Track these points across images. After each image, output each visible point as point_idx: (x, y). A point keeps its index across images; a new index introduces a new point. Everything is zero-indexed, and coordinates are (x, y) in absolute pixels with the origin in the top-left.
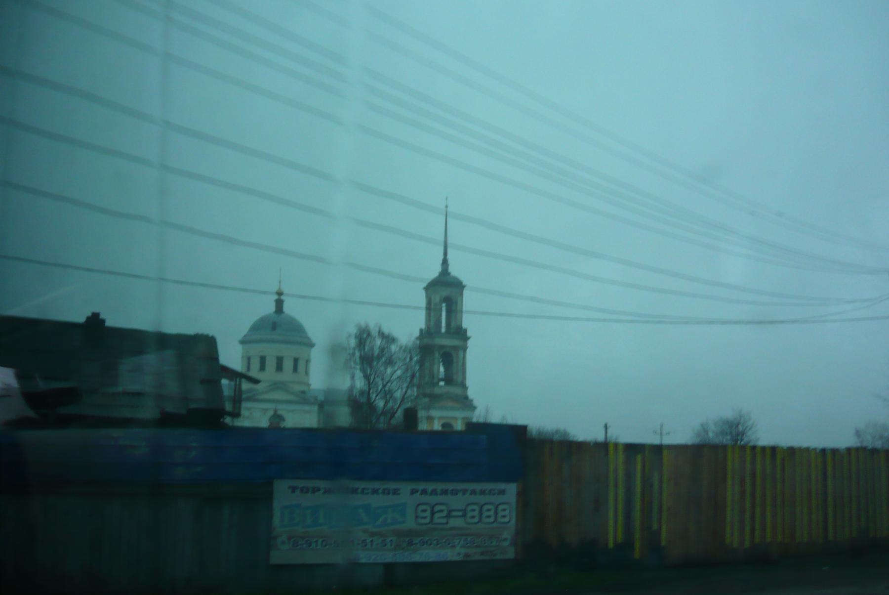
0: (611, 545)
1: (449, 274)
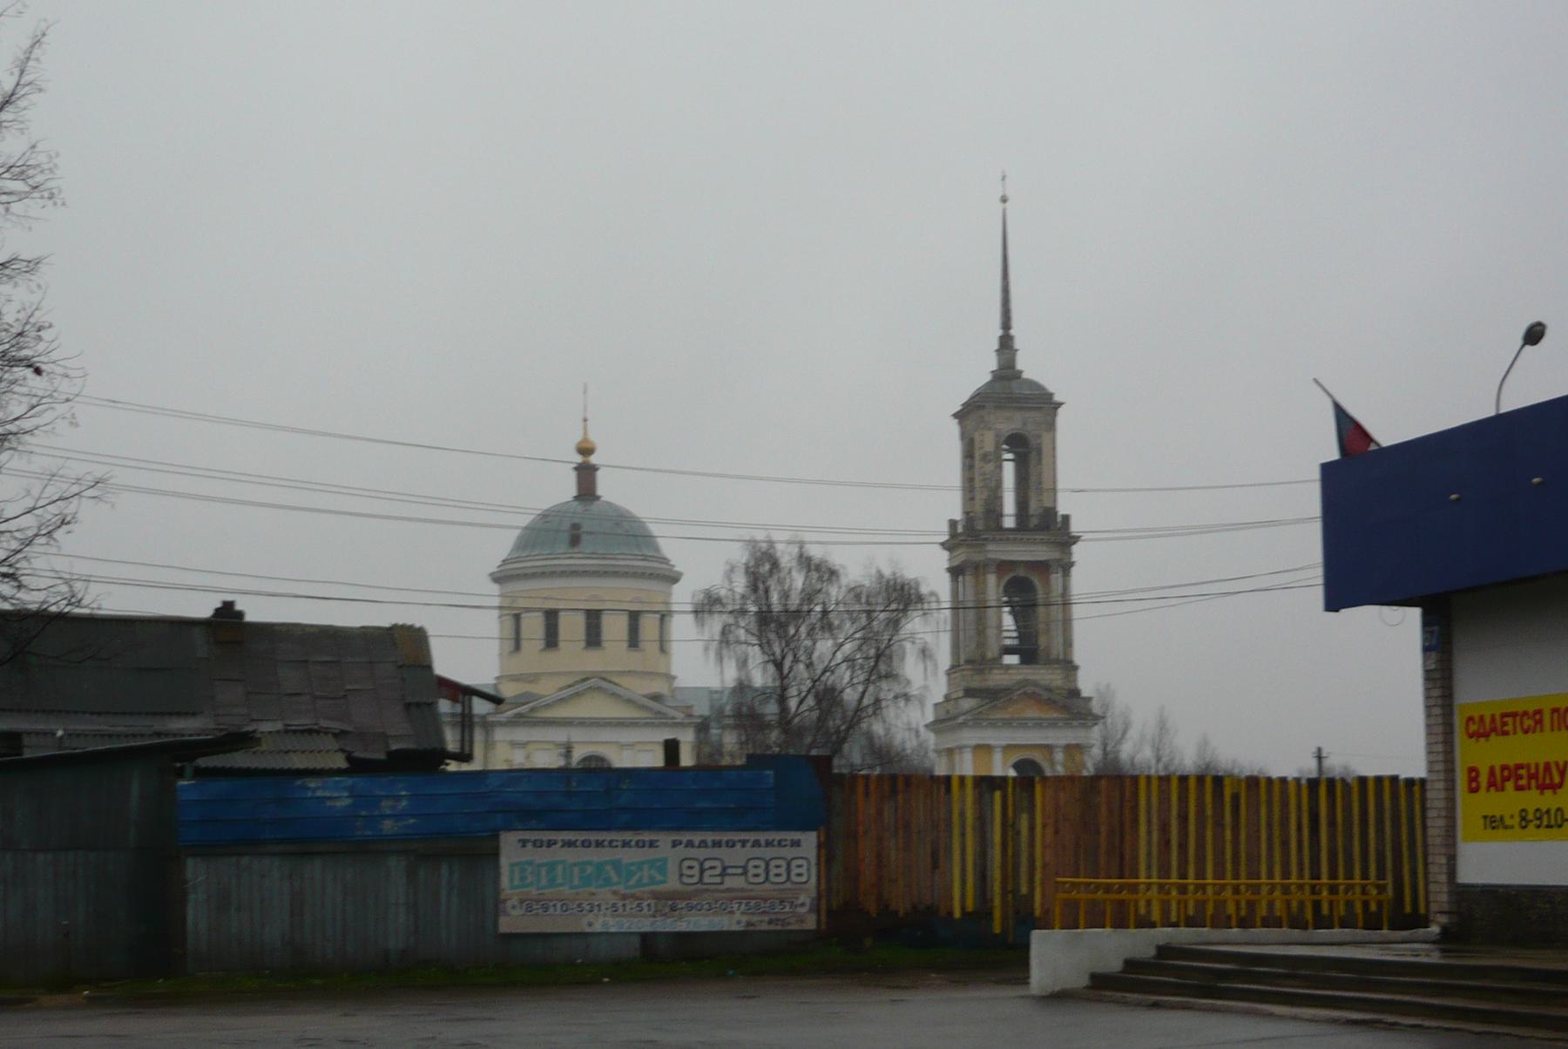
0: (957, 914)
1: (1017, 375)
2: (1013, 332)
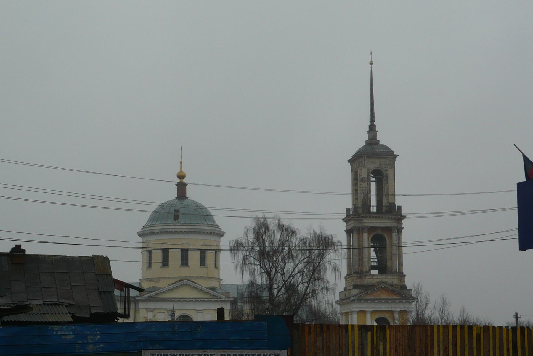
1: (377, 143)
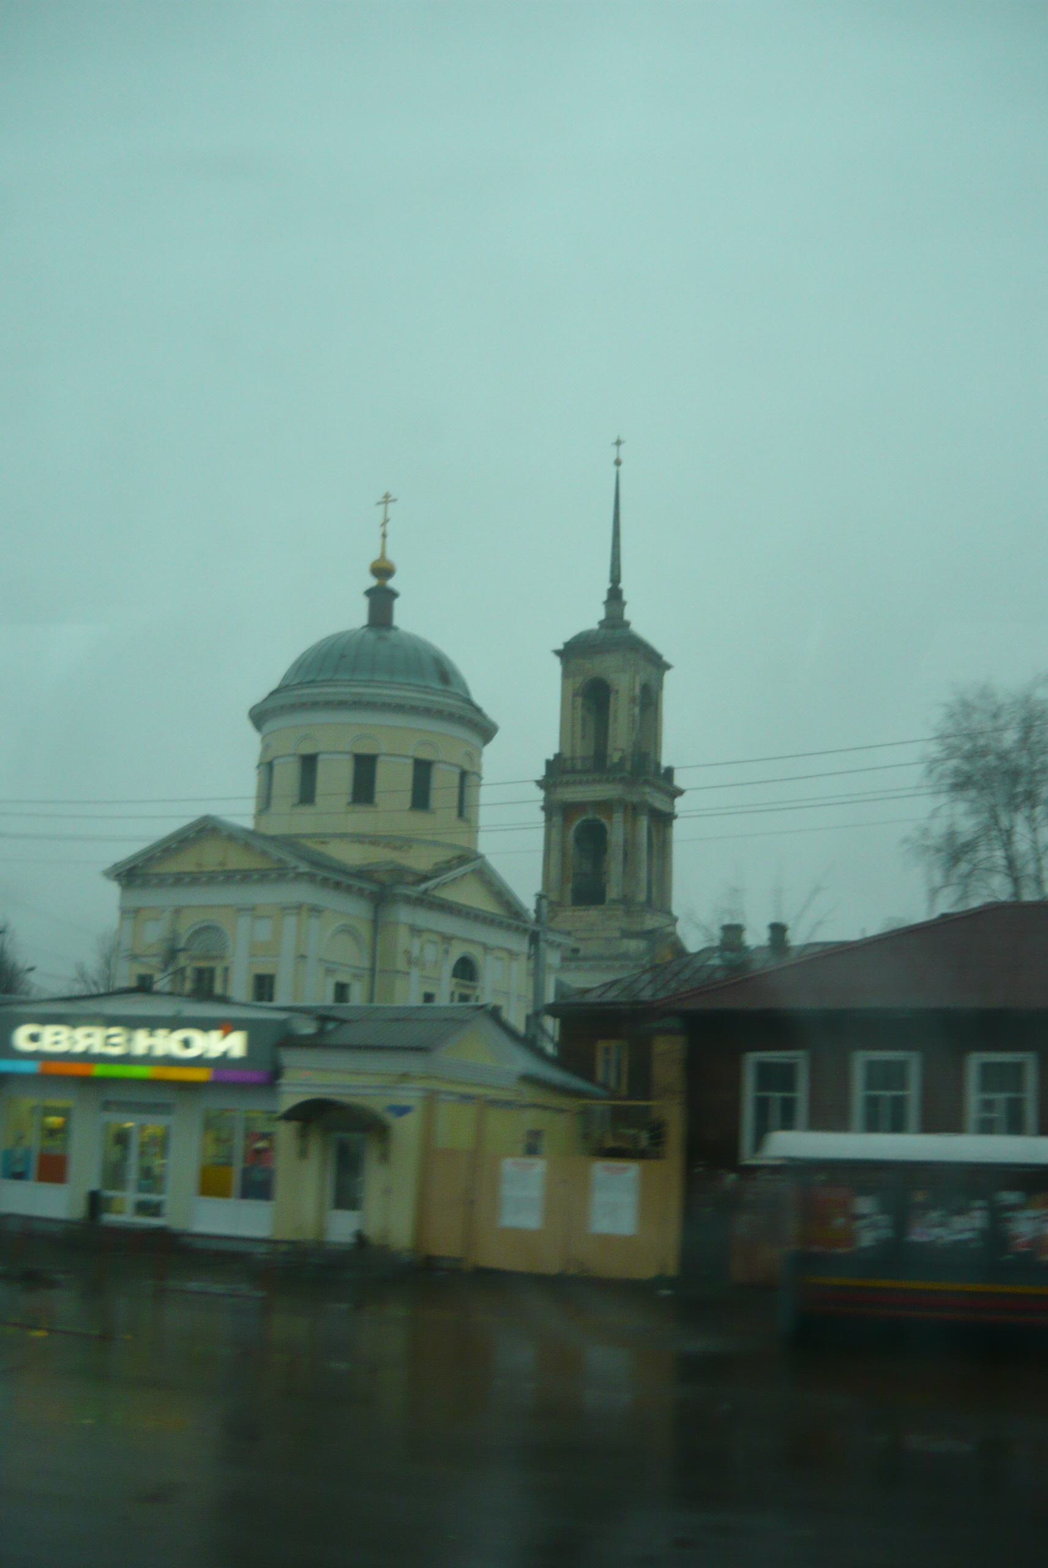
2: (622, 585)
